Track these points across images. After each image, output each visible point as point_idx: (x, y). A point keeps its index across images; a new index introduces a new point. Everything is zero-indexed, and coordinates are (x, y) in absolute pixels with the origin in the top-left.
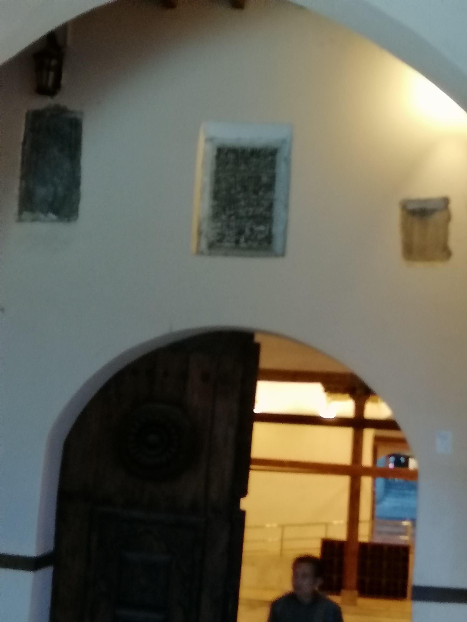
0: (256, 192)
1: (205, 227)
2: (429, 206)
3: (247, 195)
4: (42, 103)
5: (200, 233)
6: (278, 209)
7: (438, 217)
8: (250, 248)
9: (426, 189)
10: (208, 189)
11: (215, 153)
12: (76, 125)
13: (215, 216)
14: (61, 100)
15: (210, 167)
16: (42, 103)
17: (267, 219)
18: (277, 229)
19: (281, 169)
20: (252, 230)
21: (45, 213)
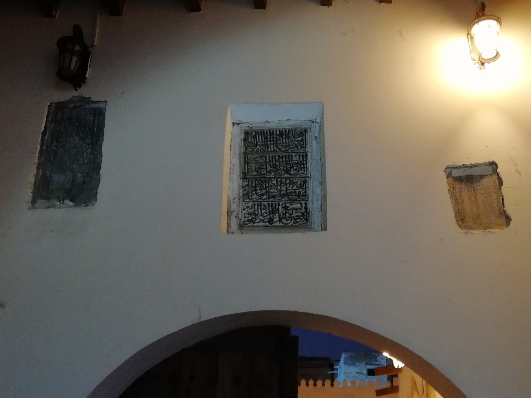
0: (287, 172)
1: (234, 207)
2: (475, 172)
3: (279, 175)
4: (66, 95)
5: (229, 213)
6: (314, 188)
7: (489, 182)
8: (285, 226)
9: (473, 151)
10: (237, 170)
11: (243, 136)
12: (99, 114)
13: (245, 196)
14: (84, 91)
15: (238, 149)
16: (66, 95)
17: (302, 196)
18: (314, 205)
19: (312, 148)
20: (286, 208)
21: (61, 200)
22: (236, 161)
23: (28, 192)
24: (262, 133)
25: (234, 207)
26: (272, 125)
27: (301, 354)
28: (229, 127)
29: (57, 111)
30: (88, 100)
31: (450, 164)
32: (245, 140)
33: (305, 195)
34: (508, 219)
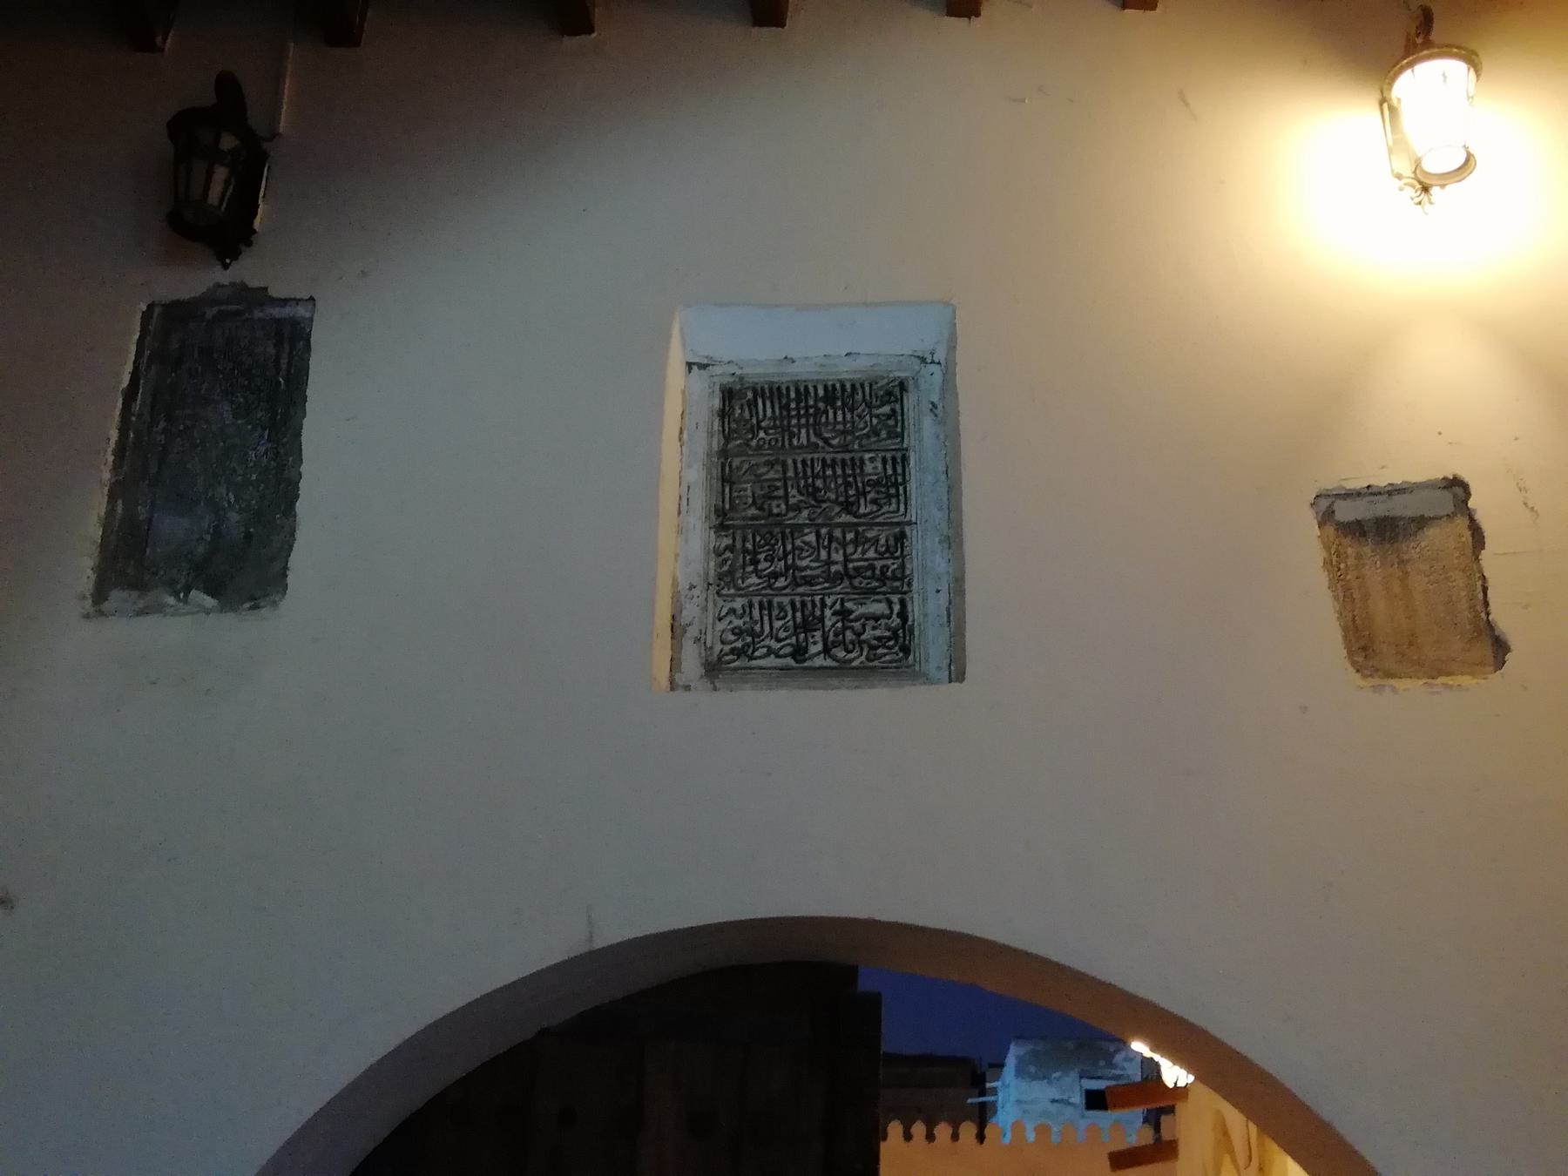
0: (848, 507)
1: (691, 611)
2: (1402, 508)
3: (825, 517)
4: (196, 280)
5: (677, 629)
6: (926, 555)
7: (1443, 538)
8: (843, 669)
9: (1398, 447)
10: (700, 502)
11: (717, 403)
12: (293, 338)
13: (725, 579)
14: (249, 270)
15: (704, 441)
16: (196, 280)
17: (892, 580)
18: (927, 607)
19: (923, 436)
20: (844, 614)
21: (181, 591)
22: (696, 475)
23: (83, 569)
24: (773, 392)
25: (691, 611)
26: (804, 370)
27: (888, 1045)
28: (676, 375)
29: (169, 328)
30: (261, 297)
31: (1330, 483)
32: (723, 414)
33: (902, 576)
34: (1501, 648)
